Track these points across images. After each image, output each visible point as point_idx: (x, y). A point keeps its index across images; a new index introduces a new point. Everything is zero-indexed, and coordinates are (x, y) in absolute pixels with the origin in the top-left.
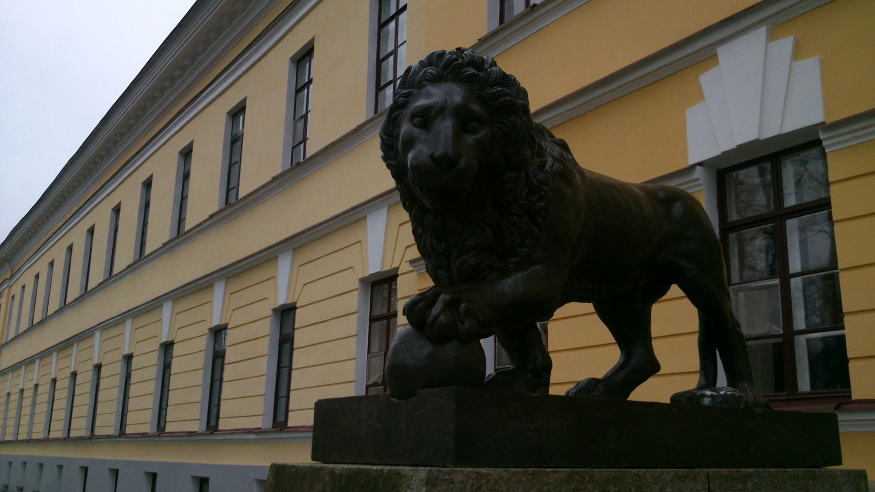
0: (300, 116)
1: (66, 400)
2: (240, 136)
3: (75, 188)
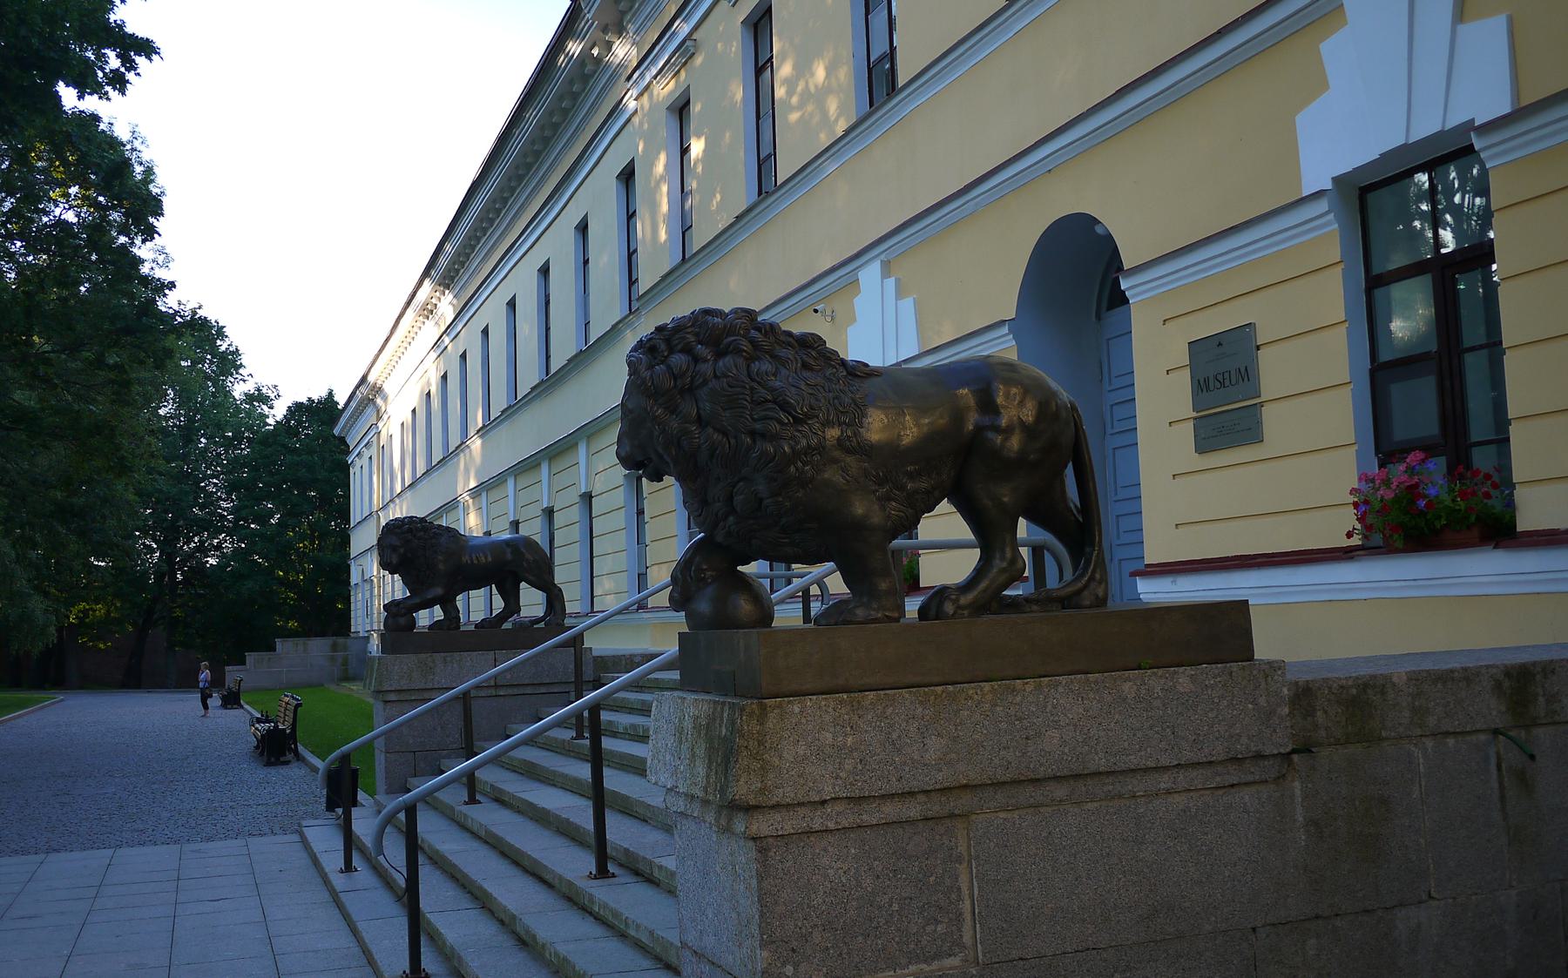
1: (1342, 331)
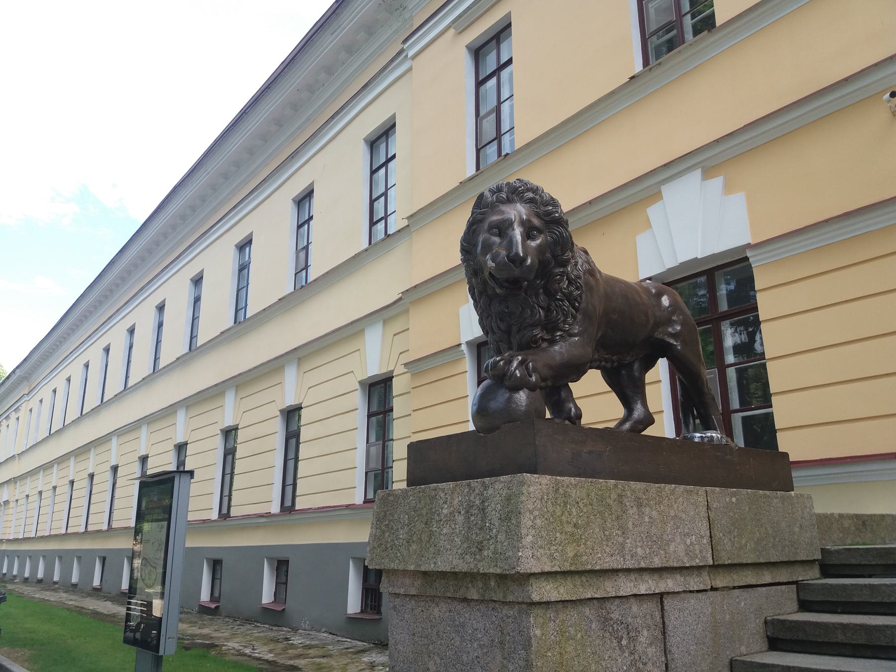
0: (303, 247)
3: (77, 326)
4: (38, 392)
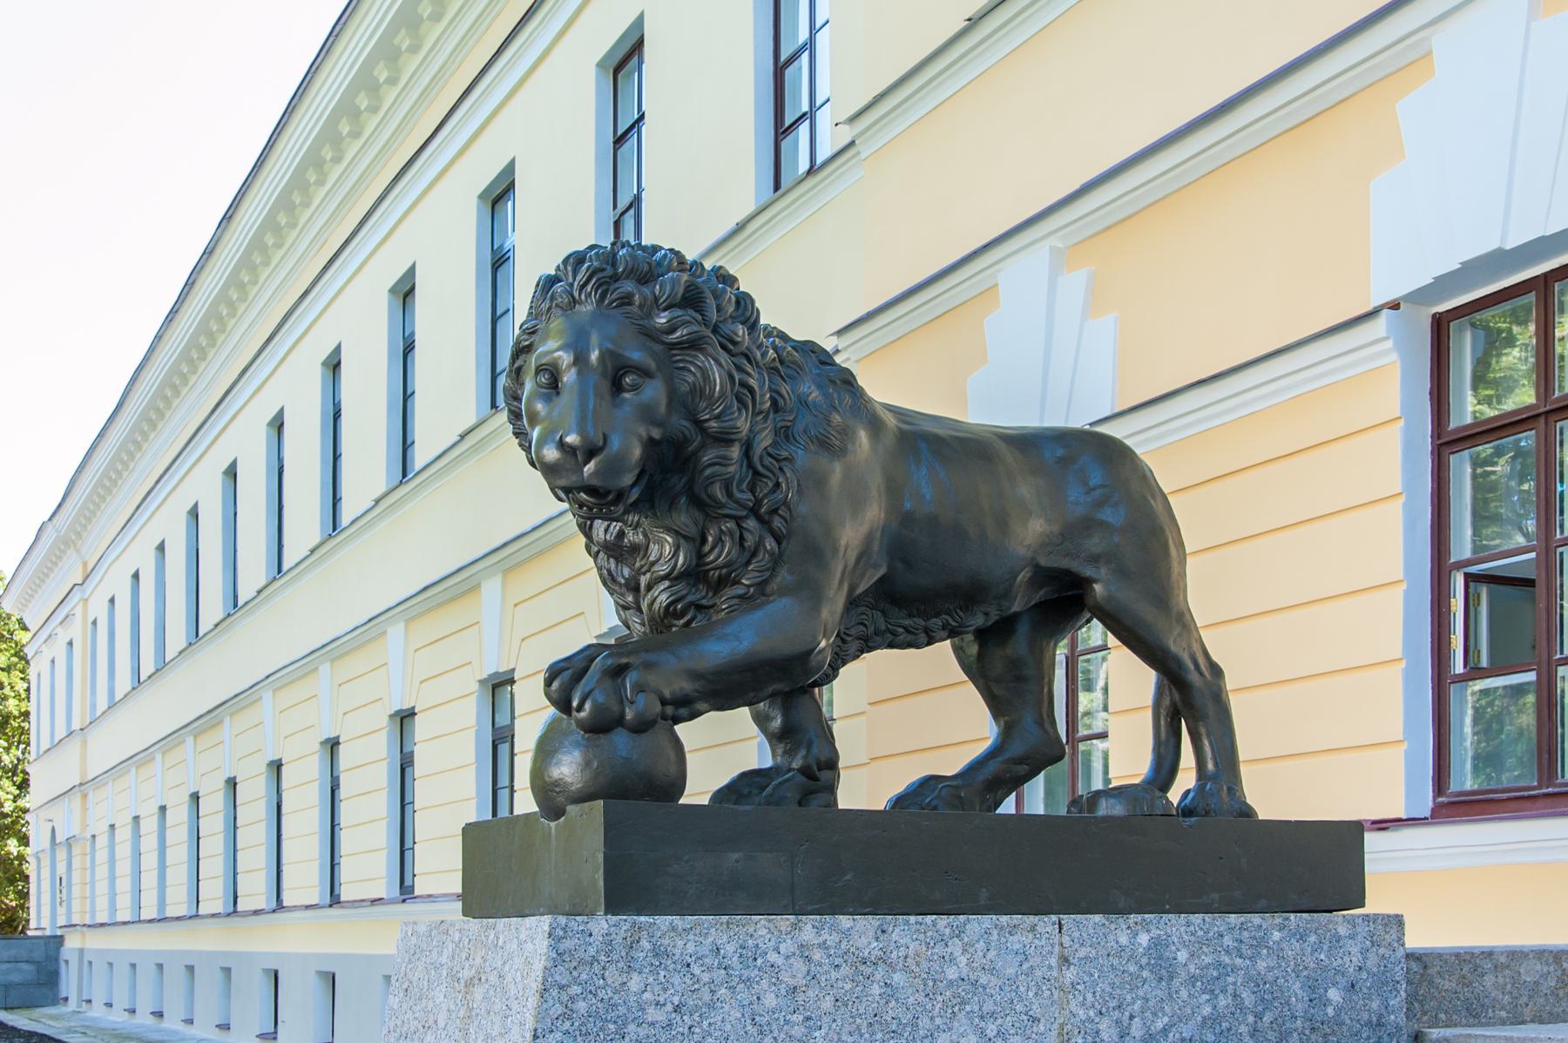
2: (509, 250)
4: (102, 578)
